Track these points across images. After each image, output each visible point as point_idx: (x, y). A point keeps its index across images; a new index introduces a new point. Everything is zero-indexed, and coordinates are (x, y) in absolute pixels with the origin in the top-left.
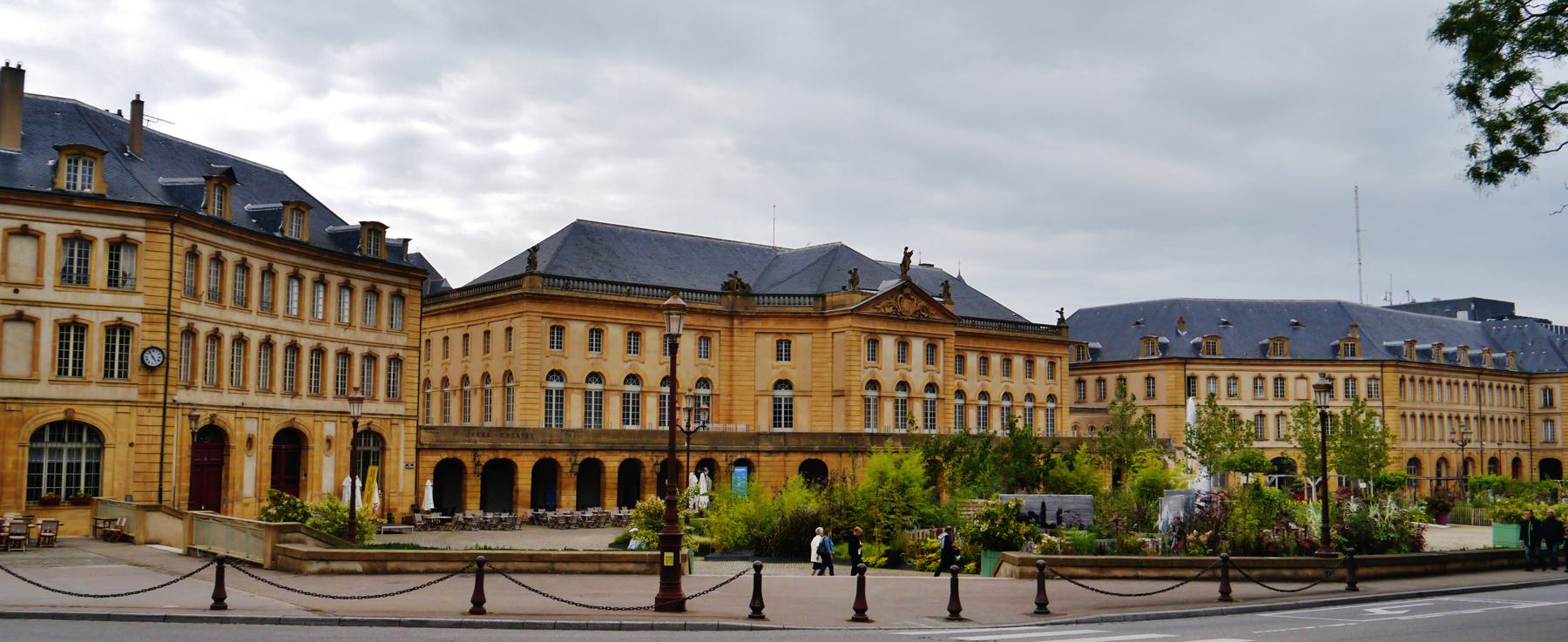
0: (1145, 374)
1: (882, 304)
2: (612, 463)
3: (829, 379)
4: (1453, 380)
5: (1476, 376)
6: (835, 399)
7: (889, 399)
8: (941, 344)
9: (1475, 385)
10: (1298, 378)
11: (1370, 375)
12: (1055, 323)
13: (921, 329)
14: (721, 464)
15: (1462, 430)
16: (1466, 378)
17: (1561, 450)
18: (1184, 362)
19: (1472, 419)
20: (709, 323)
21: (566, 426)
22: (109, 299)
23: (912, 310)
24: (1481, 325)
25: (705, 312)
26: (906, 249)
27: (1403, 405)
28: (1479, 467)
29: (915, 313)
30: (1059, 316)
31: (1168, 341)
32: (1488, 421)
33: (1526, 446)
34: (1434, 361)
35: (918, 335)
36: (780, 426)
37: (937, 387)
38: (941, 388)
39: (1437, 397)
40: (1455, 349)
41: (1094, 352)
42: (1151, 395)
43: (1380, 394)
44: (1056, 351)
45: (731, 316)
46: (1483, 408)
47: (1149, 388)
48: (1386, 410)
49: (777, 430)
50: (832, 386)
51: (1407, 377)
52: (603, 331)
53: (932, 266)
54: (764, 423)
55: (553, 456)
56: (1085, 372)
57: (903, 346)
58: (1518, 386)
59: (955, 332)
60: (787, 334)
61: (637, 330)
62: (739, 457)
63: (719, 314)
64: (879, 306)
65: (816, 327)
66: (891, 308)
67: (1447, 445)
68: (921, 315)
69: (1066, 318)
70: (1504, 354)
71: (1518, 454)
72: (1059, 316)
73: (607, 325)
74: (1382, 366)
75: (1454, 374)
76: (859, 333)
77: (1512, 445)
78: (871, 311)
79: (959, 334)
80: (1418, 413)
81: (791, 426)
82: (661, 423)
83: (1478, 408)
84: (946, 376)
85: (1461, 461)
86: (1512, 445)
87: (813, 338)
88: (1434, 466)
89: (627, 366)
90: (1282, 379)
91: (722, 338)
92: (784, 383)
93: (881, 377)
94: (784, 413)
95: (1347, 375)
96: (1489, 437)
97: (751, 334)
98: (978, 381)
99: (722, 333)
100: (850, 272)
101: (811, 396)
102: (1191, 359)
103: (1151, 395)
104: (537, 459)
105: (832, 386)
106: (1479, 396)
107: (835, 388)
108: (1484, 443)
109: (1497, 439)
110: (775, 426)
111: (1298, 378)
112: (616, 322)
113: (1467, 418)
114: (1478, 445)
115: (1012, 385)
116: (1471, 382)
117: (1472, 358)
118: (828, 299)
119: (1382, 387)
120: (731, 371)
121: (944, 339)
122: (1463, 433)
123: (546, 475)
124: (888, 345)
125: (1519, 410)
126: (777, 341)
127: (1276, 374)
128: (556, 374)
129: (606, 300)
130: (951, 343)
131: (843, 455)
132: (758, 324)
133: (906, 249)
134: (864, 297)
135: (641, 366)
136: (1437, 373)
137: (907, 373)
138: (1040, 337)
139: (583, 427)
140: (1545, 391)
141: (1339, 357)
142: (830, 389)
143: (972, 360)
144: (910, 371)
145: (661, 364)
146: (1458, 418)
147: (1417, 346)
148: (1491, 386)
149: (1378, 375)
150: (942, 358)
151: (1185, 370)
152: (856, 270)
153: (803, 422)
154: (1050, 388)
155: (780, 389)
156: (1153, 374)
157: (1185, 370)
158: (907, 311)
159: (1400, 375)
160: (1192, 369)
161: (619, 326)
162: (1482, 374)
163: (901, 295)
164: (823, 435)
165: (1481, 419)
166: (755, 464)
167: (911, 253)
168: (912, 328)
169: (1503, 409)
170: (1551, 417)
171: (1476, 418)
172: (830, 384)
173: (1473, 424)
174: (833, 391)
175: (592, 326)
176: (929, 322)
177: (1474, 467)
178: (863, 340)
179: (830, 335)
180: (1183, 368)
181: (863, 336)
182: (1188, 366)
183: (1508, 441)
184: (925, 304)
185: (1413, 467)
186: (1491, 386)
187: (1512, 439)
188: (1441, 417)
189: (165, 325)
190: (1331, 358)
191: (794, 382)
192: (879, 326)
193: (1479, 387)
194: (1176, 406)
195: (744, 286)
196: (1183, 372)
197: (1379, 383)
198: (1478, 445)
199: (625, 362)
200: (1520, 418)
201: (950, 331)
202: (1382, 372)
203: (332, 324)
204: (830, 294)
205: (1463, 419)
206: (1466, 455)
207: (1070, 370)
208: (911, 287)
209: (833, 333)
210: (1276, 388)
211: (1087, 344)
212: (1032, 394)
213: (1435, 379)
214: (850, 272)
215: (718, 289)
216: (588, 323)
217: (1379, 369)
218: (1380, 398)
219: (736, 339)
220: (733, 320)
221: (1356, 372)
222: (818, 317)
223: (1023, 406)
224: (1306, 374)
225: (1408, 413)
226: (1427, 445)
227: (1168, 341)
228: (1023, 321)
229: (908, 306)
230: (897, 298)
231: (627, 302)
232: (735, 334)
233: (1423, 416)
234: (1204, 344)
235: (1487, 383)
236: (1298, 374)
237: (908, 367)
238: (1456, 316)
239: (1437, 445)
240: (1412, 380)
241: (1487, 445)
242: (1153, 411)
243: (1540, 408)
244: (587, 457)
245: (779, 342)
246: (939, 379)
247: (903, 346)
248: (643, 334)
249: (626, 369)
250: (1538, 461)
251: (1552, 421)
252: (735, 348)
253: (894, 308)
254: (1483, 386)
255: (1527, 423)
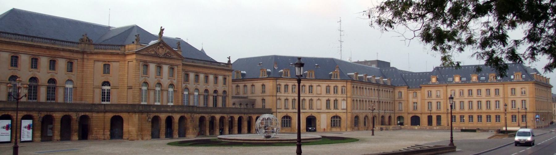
0: (262, 84)
1: (149, 50)
2: (58, 116)
3: (126, 81)
4: (370, 88)
5: (378, 86)
6: (129, 90)
7: (152, 90)
8: (75, 63)
9: (377, 90)
10: (317, 86)
11: (342, 85)
12: (227, 62)
13: (167, 61)
14: (74, 117)
15: (373, 105)
16: (374, 87)
17: (404, 113)
18: (276, 79)
19: (376, 102)
20: (72, 56)
21: (266, 108)
22: (292, 95)
23: (163, 53)
24: (379, 69)
25: (70, 51)
26: (161, 27)
27: (354, 96)
28: (378, 119)
29: (164, 54)
30: (228, 60)
31: (270, 71)
32: (381, 103)
33: (393, 112)
34: (364, 81)
35: (165, 64)
36: (105, 101)
37: (174, 86)
38: (175, 86)
39: (365, 94)
40: (371, 77)
41: (243, 75)
42: (263, 92)
43: (346, 92)
44: (227, 73)
45: (83, 53)
46: (380, 98)
47: (263, 89)
48: (348, 98)
49: (103, 103)
50: (127, 84)
51: (355, 86)
52: (56, 61)
53: (180, 39)
54: (97, 100)
55: (51, 113)
56: (240, 82)
57: (159, 67)
58: (391, 91)
59: (183, 64)
60: (108, 61)
61: (37, 57)
62: (83, 114)
63: (77, 52)
64: (148, 51)
65: (121, 59)
66: (154, 52)
67: (368, 111)
68: (167, 55)
69: (232, 62)
70: (387, 79)
71: (390, 114)
72: (228, 60)
73: (20, 54)
74: (347, 82)
75: (370, 86)
76: (139, 62)
77: (389, 111)
78: (145, 53)
79: (183, 65)
80: (368, 100)
81: (109, 101)
82: (204, 104)
83: (378, 98)
84: (178, 81)
85: (372, 116)
86: (389, 111)
87: (120, 64)
88: (363, 119)
89: (30, 73)
90: (312, 86)
91: (79, 63)
92: (106, 83)
93: (149, 80)
94: (106, 96)
95: (335, 85)
96: (381, 109)
97: (92, 61)
98: (194, 84)
99: (79, 60)
100: (136, 36)
101: (118, 89)
102: (279, 78)
103: (263, 92)
104: (63, 115)
105: (127, 84)
106: (379, 94)
107: (129, 86)
108: (380, 111)
109: (384, 109)
110: (102, 101)
111: (317, 86)
112: (25, 53)
113: (374, 102)
114: (378, 111)
115: (208, 87)
116: (376, 89)
117: (376, 80)
118: (127, 47)
119: (347, 90)
120: (83, 77)
121: (177, 66)
122: (373, 106)
123: (66, 121)
124: (152, 67)
125: (391, 99)
126: (104, 65)
127: (310, 84)
128: (106, 83)
129: (20, 43)
130: (181, 68)
131: (130, 114)
132: (95, 57)
133: (161, 27)
134: (142, 47)
135: (37, 73)
136: (365, 85)
137: (173, 80)
138: (220, 67)
139: (7, 100)
140: (399, 92)
141: (332, 78)
142: (126, 86)
143: (192, 76)
144: (162, 79)
145: (48, 73)
146: (372, 101)
147: (359, 75)
148: (382, 90)
149: (345, 85)
150: (176, 75)
151: (276, 82)
152: (139, 35)
153: (114, 100)
154: (224, 88)
155: (105, 86)
156: (265, 84)
157: (276, 82)
158: (161, 54)
159: (353, 85)
160: (279, 82)
161: (27, 55)
162: (379, 86)
163: (159, 47)
164: (122, 105)
165: (379, 102)
166: (90, 117)
167: (163, 29)
168: (163, 60)
169: (386, 99)
170: (401, 102)
171: (377, 102)
172: (126, 83)
173: (376, 103)
174: (128, 87)
175: (13, 55)
176: (170, 58)
177: (376, 119)
178: (141, 64)
179: (127, 63)
180: (276, 81)
181: (141, 63)
182: (278, 81)
183: (387, 110)
184: (169, 51)
185: (356, 119)
186: (382, 90)
187: (389, 109)
188: (366, 101)
189: (452, 113)
190: (329, 78)
191: (111, 83)
192: (148, 59)
193: (379, 90)
194: (273, 96)
195: (89, 41)
196: (275, 83)
197: (345, 88)
198: (378, 111)
199: (30, 71)
200: (391, 102)
201: (180, 62)
202: (347, 84)
203: (283, 93)
204: (127, 45)
205: (373, 102)
206: (374, 115)
207: (232, 82)
208: (163, 44)
209: (128, 62)
210: (310, 89)
211: (240, 71)
212: (217, 90)
213: (364, 87)
214: (136, 36)
215: (77, 41)
216: (10, 53)
217: (345, 83)
218: (346, 94)
219: (85, 63)
220: (84, 55)
221: (338, 84)
222: (122, 55)
223: (101, 88)
224: (320, 85)
225: (355, 99)
226: (361, 111)
227: (270, 71)
228: (214, 61)
229: (161, 52)
230: (156, 48)
231: (31, 45)
232: (85, 61)
233: (369, 101)
234: (284, 72)
235: (381, 89)
236: (318, 84)
237: (161, 77)
238: (371, 66)
239: (364, 111)
240: (357, 87)
241: (381, 111)
242: (265, 98)
243: (398, 98)
244: (4, 114)
245: (105, 65)
246: (175, 82)
247: (159, 67)
248: (39, 59)
249: (49, 77)
250: (397, 117)
251: (401, 103)
252: (84, 67)
253: (155, 52)
254: (380, 90)
255: (393, 104)
